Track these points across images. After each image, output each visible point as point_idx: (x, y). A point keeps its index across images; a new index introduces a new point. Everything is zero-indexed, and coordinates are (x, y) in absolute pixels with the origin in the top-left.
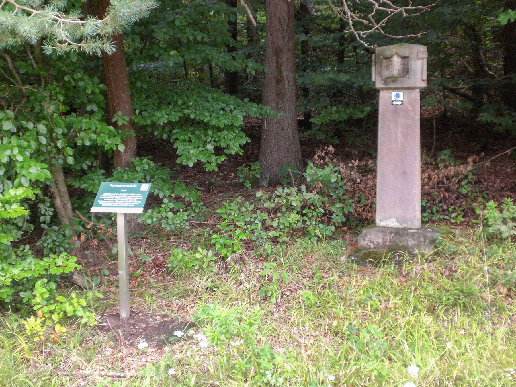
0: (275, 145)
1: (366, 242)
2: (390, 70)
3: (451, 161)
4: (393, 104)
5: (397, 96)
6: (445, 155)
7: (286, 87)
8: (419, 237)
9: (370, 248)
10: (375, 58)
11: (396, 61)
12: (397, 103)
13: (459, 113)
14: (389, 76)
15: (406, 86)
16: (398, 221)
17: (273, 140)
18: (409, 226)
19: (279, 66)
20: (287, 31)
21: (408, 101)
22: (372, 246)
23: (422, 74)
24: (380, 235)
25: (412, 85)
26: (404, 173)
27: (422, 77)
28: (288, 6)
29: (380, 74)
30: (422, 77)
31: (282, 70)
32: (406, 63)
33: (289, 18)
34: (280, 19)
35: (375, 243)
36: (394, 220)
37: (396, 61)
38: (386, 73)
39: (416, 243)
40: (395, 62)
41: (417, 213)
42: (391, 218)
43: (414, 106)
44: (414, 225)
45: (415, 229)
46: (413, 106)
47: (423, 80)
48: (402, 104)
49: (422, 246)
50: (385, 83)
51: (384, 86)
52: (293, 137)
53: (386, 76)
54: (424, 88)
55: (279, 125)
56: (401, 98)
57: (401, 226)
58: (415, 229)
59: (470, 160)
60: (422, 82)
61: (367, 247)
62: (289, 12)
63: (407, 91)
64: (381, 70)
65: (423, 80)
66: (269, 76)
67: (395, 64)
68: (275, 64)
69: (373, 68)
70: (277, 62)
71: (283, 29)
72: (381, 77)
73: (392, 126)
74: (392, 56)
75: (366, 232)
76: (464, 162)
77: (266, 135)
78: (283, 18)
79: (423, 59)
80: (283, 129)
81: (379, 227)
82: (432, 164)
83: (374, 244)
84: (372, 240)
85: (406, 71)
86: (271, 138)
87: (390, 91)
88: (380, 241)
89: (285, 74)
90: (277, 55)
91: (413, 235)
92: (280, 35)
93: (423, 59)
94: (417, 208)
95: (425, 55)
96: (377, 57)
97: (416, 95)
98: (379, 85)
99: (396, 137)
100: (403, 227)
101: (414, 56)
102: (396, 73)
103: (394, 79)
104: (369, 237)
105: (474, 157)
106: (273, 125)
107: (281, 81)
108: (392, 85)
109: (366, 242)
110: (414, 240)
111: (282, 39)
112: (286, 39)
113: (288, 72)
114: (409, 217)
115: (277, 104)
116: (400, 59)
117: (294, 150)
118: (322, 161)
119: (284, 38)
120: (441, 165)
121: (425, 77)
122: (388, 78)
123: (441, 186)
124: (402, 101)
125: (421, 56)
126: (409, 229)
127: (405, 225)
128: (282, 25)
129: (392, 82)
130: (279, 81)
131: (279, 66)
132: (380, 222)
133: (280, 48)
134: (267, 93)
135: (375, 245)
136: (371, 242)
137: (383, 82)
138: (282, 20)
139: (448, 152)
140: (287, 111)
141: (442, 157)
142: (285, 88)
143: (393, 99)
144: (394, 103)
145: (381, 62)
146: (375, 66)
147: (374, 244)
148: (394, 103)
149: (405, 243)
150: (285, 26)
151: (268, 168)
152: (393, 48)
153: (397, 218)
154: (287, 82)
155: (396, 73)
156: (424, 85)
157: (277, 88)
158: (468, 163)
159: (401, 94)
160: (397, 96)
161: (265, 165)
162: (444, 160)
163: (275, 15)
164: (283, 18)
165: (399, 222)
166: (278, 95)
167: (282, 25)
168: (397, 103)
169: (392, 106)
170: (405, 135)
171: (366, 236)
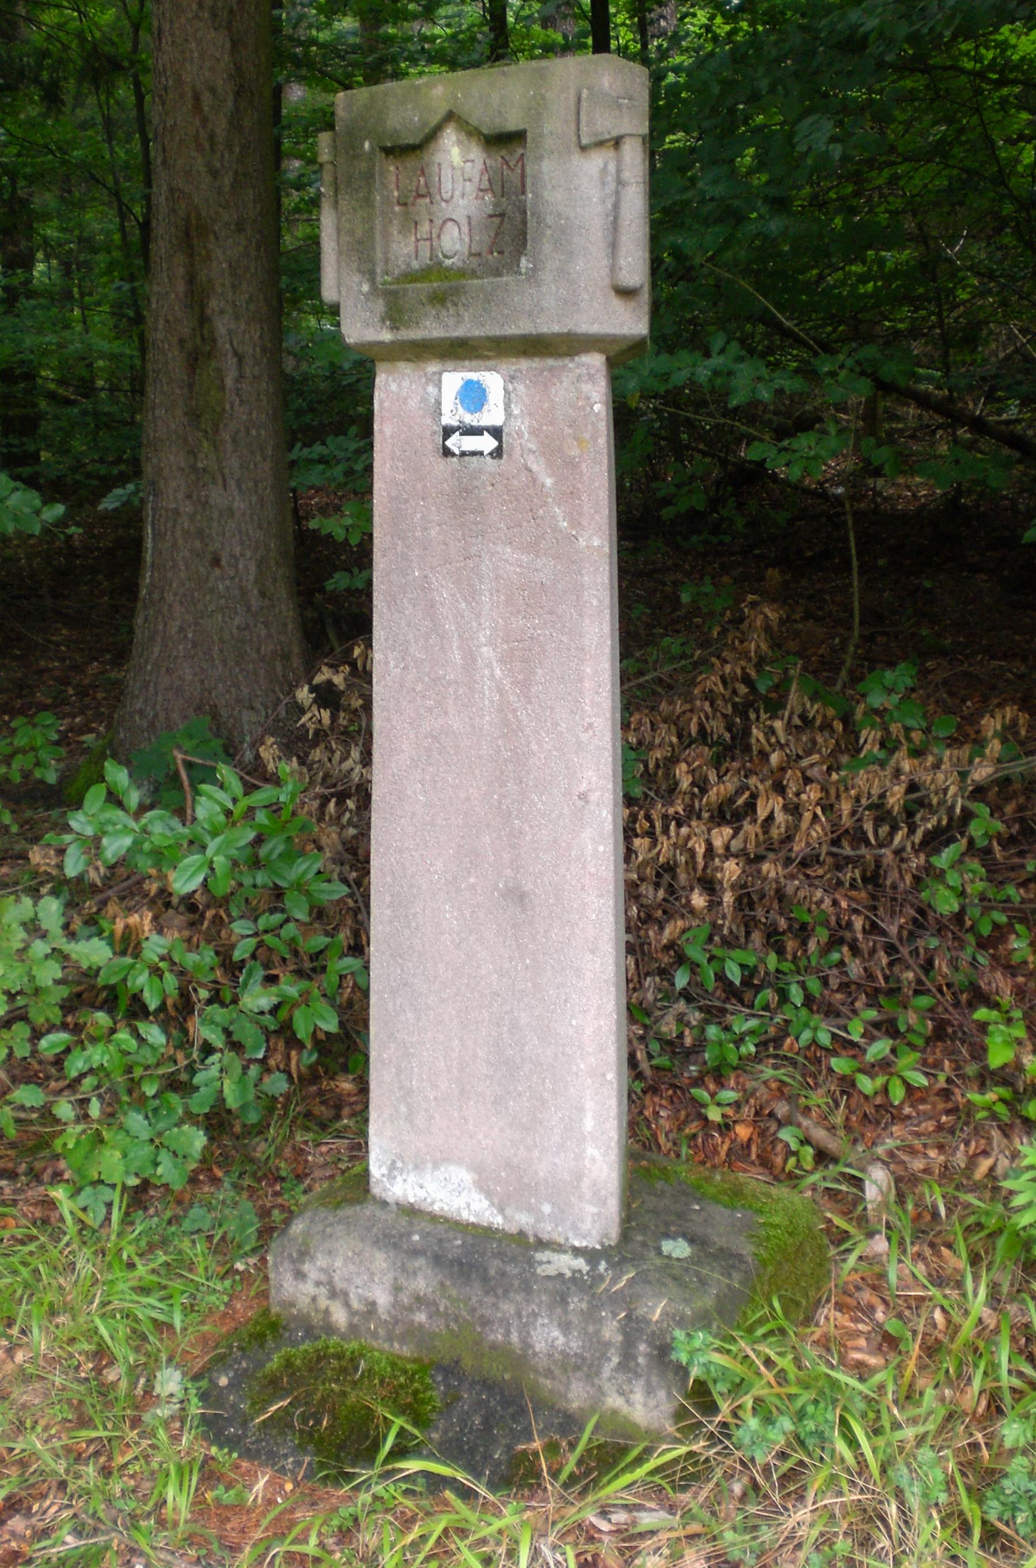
0: (181, 629)
1: (309, 1288)
2: (425, 228)
3: (911, 723)
4: (447, 452)
5: (474, 396)
6: (886, 690)
7: (229, 382)
8: (591, 1316)
9: (330, 1329)
10: (334, 147)
11: (458, 164)
12: (470, 443)
13: (1005, 498)
14: (415, 265)
15: (512, 330)
16: (483, 1187)
17: (178, 609)
18: (547, 1230)
19: (197, 297)
20: (230, 148)
21: (534, 432)
22: (340, 1317)
23: (613, 246)
24: (380, 1260)
25: (549, 326)
26: (518, 896)
27: (613, 268)
28: (235, 45)
29: (362, 252)
30: (613, 268)
31: (208, 311)
32: (515, 178)
33: (238, 94)
34: (197, 98)
35: (355, 1305)
36: (462, 1175)
37: (458, 164)
38: (404, 251)
39: (575, 1345)
40: (446, 174)
41: (591, 1151)
42: (446, 1160)
43: (572, 465)
44: (575, 1228)
45: (577, 1252)
46: (567, 467)
47: (625, 293)
48: (497, 453)
49: (607, 1371)
50: (395, 314)
51: (387, 336)
52: (263, 594)
53: (400, 265)
54: (637, 346)
55: (198, 544)
56: (492, 415)
57: (498, 1221)
58: (577, 1252)
59: (991, 725)
60: (617, 304)
61: (316, 1319)
62: (238, 68)
63: (524, 364)
64: (370, 232)
65: (625, 293)
66: (160, 335)
67: (447, 186)
68: (181, 287)
69: (328, 221)
70: (191, 279)
71: (211, 137)
72: (371, 275)
73: (444, 592)
74: (433, 135)
75: (307, 1234)
76: (967, 736)
77: (152, 585)
78: (213, 90)
79: (617, 142)
80: (216, 562)
81: (384, 1204)
82: (826, 726)
83: (347, 1305)
84: (340, 1285)
85: (512, 229)
86: (169, 597)
87: (432, 367)
88: (383, 1298)
89: (221, 326)
90: (191, 247)
91: (563, 1287)
92: (200, 165)
93: (617, 142)
94: (589, 1124)
95: (635, 123)
96: (348, 146)
97: (587, 391)
98: (361, 327)
99: (470, 657)
100: (513, 1229)
101: (554, 126)
102: (454, 242)
103: (442, 284)
104: (322, 1261)
105: (1009, 712)
106: (175, 544)
107: (209, 356)
108: (432, 328)
109: (309, 1288)
110: (566, 1327)
111: (208, 179)
112: (227, 181)
113: (237, 318)
114: (542, 1170)
115: (192, 453)
116: (477, 153)
117: (267, 648)
118: (326, 715)
119: (214, 173)
120: (869, 737)
121: (634, 268)
122: (411, 277)
123: (847, 850)
124: (496, 433)
125: (606, 124)
126: (542, 1244)
127: (522, 1220)
128: (205, 121)
129: (455, 313)
130: (199, 355)
131: (197, 297)
132: (391, 1177)
133: (199, 217)
134: (153, 409)
135: (352, 1313)
136: (333, 1294)
137: (380, 306)
138: (207, 99)
139: (901, 676)
140: (232, 484)
141: (876, 700)
142: (222, 388)
143: (447, 420)
144: (454, 442)
145: (369, 176)
146: (336, 204)
147: (347, 1305)
148: (454, 442)
149: (515, 1337)
150: (221, 125)
151: (152, 724)
152: (430, 86)
153: (477, 1168)
154: (232, 362)
155: (454, 242)
156: (632, 322)
157: (190, 386)
158: (980, 743)
159: (493, 381)
160: (474, 396)
161: (141, 712)
162: (879, 712)
163: (180, 81)
164: (213, 90)
165: (489, 1194)
166: (194, 416)
167: (205, 121)
168: (470, 443)
169: (442, 467)
170: (522, 656)
171: (304, 1254)
